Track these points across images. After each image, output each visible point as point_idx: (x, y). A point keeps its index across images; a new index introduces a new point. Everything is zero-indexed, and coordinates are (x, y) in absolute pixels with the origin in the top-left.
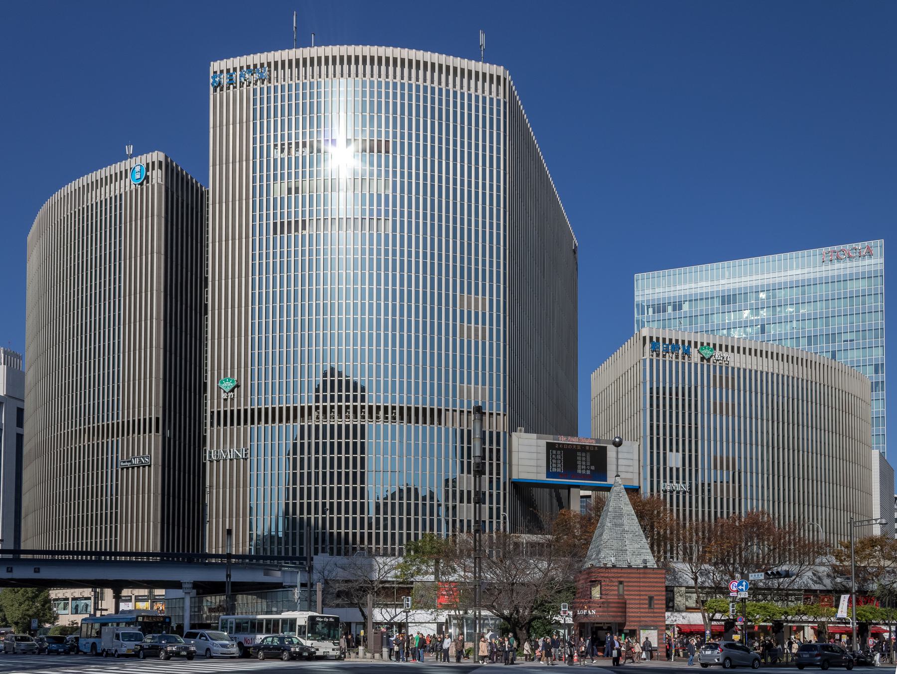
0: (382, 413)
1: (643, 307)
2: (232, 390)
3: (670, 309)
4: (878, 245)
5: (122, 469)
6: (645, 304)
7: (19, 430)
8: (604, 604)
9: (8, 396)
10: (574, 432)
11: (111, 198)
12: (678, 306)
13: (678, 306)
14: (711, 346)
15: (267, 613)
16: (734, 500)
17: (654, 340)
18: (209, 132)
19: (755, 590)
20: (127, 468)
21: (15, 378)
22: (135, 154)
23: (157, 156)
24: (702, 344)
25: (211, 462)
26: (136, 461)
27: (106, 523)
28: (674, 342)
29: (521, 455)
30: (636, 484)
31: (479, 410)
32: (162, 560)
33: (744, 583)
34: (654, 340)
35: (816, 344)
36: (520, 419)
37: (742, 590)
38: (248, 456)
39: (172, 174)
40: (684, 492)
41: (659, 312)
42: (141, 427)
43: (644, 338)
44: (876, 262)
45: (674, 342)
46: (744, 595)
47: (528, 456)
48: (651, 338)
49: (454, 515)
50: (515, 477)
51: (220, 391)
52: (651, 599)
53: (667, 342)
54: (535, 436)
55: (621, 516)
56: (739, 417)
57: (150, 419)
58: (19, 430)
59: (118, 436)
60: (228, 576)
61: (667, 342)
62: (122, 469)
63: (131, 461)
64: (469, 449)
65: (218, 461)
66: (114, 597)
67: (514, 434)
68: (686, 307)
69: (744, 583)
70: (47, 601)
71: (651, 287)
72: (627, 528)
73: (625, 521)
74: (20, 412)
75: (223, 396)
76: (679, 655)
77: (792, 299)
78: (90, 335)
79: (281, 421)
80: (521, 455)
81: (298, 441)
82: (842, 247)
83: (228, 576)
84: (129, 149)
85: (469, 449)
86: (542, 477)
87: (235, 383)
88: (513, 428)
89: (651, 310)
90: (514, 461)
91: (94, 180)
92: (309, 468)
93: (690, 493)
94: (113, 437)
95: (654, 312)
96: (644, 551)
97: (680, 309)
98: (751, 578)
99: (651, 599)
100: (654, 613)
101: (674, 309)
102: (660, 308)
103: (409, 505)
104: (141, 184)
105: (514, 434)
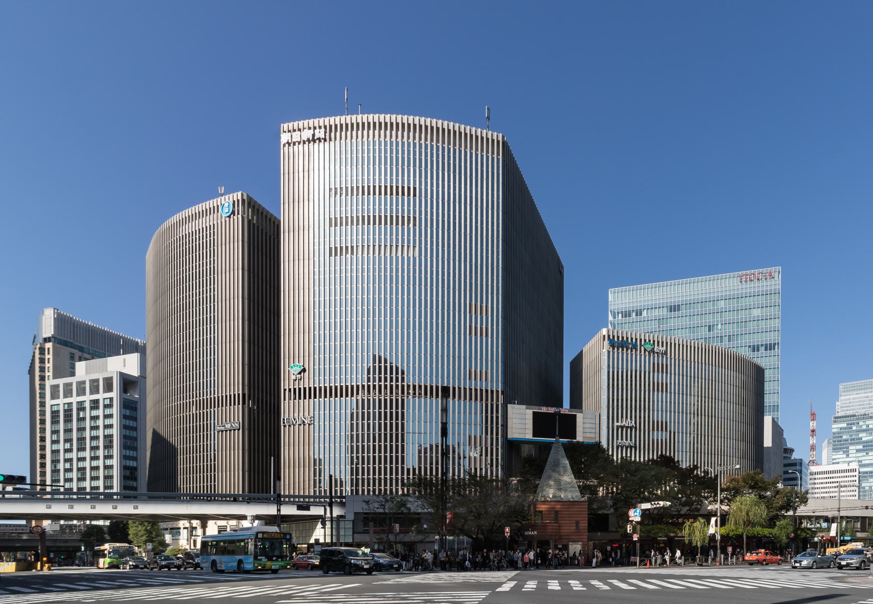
2: (300, 373)
3: (634, 314)
4: (776, 270)
12: (639, 313)
13: (639, 313)
15: (71, 526)
19: (644, 513)
22: (227, 192)
23: (237, 196)
24: (645, 340)
25: (285, 426)
26: (228, 426)
29: (515, 421)
30: (597, 440)
31: (445, 390)
36: (513, 392)
39: (250, 204)
40: (631, 447)
42: (231, 400)
44: (776, 283)
47: (521, 422)
48: (609, 336)
49: (403, 463)
50: (510, 436)
51: (289, 374)
54: (524, 406)
60: (279, 510)
65: (289, 426)
68: (644, 313)
70: (159, 529)
71: (619, 299)
77: (758, 304)
79: (347, 396)
81: (355, 411)
83: (279, 510)
86: (529, 435)
88: (508, 401)
89: (620, 315)
91: (208, 208)
92: (357, 430)
97: (641, 314)
101: (637, 315)
102: (627, 314)
103: (374, 457)
104: (229, 217)
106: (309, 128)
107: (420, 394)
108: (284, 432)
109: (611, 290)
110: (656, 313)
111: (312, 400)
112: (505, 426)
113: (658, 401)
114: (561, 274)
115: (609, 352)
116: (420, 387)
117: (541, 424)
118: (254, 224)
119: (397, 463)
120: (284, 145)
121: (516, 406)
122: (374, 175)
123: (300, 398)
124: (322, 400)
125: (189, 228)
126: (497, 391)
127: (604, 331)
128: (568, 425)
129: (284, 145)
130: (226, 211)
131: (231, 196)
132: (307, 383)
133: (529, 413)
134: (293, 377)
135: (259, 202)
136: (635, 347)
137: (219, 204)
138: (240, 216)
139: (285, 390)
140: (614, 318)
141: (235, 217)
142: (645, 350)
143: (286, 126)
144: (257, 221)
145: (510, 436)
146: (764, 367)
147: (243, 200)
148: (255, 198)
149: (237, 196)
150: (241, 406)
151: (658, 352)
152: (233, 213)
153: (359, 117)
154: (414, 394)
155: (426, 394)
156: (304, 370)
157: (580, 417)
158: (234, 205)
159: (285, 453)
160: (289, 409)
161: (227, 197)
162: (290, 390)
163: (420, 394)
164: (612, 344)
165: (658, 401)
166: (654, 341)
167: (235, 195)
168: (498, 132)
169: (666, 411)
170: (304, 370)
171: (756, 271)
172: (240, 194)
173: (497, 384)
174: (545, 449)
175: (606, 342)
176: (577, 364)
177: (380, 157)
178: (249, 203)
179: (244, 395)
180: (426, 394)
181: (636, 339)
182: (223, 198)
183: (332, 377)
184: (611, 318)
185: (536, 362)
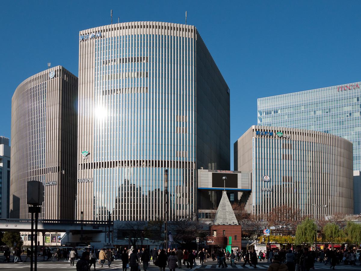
0: (145, 163)
1: (261, 112)
2: (87, 156)
3: (273, 112)
5: (46, 186)
6: (262, 111)
7: (8, 169)
8: (217, 239)
9: (4, 156)
10: (213, 173)
11: (42, 75)
14: (282, 132)
16: (270, 199)
17: (257, 130)
18: (79, 57)
19: (272, 232)
20: (48, 186)
21: (7, 150)
22: (52, 66)
23: (58, 67)
24: (278, 131)
27: (117, 53)
28: (266, 131)
30: (250, 189)
32: (61, 222)
33: (268, 230)
34: (257, 130)
35: (343, 124)
37: (268, 233)
38: (93, 181)
39: (64, 72)
41: (268, 114)
42: (52, 170)
43: (253, 130)
45: (266, 131)
46: (268, 234)
47: (206, 179)
48: (256, 130)
50: (199, 187)
52: (236, 236)
53: (263, 131)
55: (225, 206)
56: (294, 160)
57: (56, 167)
58: (8, 169)
59: (44, 174)
60: (82, 228)
61: (263, 131)
62: (46, 186)
63: (49, 183)
64: (94, 211)
66: (43, 235)
67: (199, 170)
68: (279, 112)
69: (268, 230)
72: (227, 210)
73: (227, 208)
74: (9, 162)
75: (83, 158)
76: (105, 246)
78: (38, 111)
80: (202, 178)
82: (346, 85)
83: (82, 228)
84: (49, 65)
85: (94, 211)
86: (210, 186)
87: (88, 153)
88: (198, 167)
89: (264, 113)
90: (199, 181)
93: (273, 192)
94: (42, 174)
95: (266, 114)
96: (234, 219)
97: (277, 112)
98: (271, 229)
99: (236, 236)
100: (237, 241)
101: (275, 113)
102: (268, 113)
104: (53, 78)
105: (199, 170)
106: (94, 32)
107: (150, 165)
108: (79, 185)
109: (259, 100)
110: (286, 111)
111: (109, 168)
112: (197, 182)
113: (294, 165)
114: (228, 94)
115: (256, 139)
116: (150, 161)
117: (216, 179)
118: (67, 82)
119: (125, 208)
120: (81, 42)
121: (202, 170)
122: (126, 52)
123: (89, 168)
124: (103, 169)
125: (33, 85)
126: (192, 163)
127: (253, 127)
128: (233, 180)
129: (81, 42)
130: (51, 75)
131: (54, 68)
132: (90, 161)
133: (210, 174)
134: (83, 158)
135: (73, 74)
136: (271, 134)
137: (48, 72)
138: (58, 78)
139: (79, 164)
140: (261, 115)
141: (56, 78)
142: (278, 137)
143: (82, 32)
144: (68, 80)
145: (199, 187)
146: (352, 142)
147: (60, 70)
148: (66, 68)
149: (58, 67)
150: (57, 173)
151: (285, 137)
152: (55, 76)
153: (119, 24)
154: (147, 165)
155: (153, 165)
156: (89, 154)
157: (239, 175)
158: (55, 72)
159: (79, 197)
160: (81, 174)
161: (52, 68)
162: (82, 164)
163: (150, 165)
164: (258, 134)
165: (289, 165)
166: (283, 131)
167: (56, 67)
168: (192, 25)
169: (301, 171)
170: (89, 154)
171: (348, 85)
172: (58, 67)
173: (192, 159)
174: (219, 194)
175: (255, 132)
176: (236, 145)
177: (129, 43)
178: (63, 71)
179: (59, 167)
180: (153, 165)
181: (272, 131)
182: (50, 69)
183: (106, 157)
184: (259, 115)
185: (214, 144)
